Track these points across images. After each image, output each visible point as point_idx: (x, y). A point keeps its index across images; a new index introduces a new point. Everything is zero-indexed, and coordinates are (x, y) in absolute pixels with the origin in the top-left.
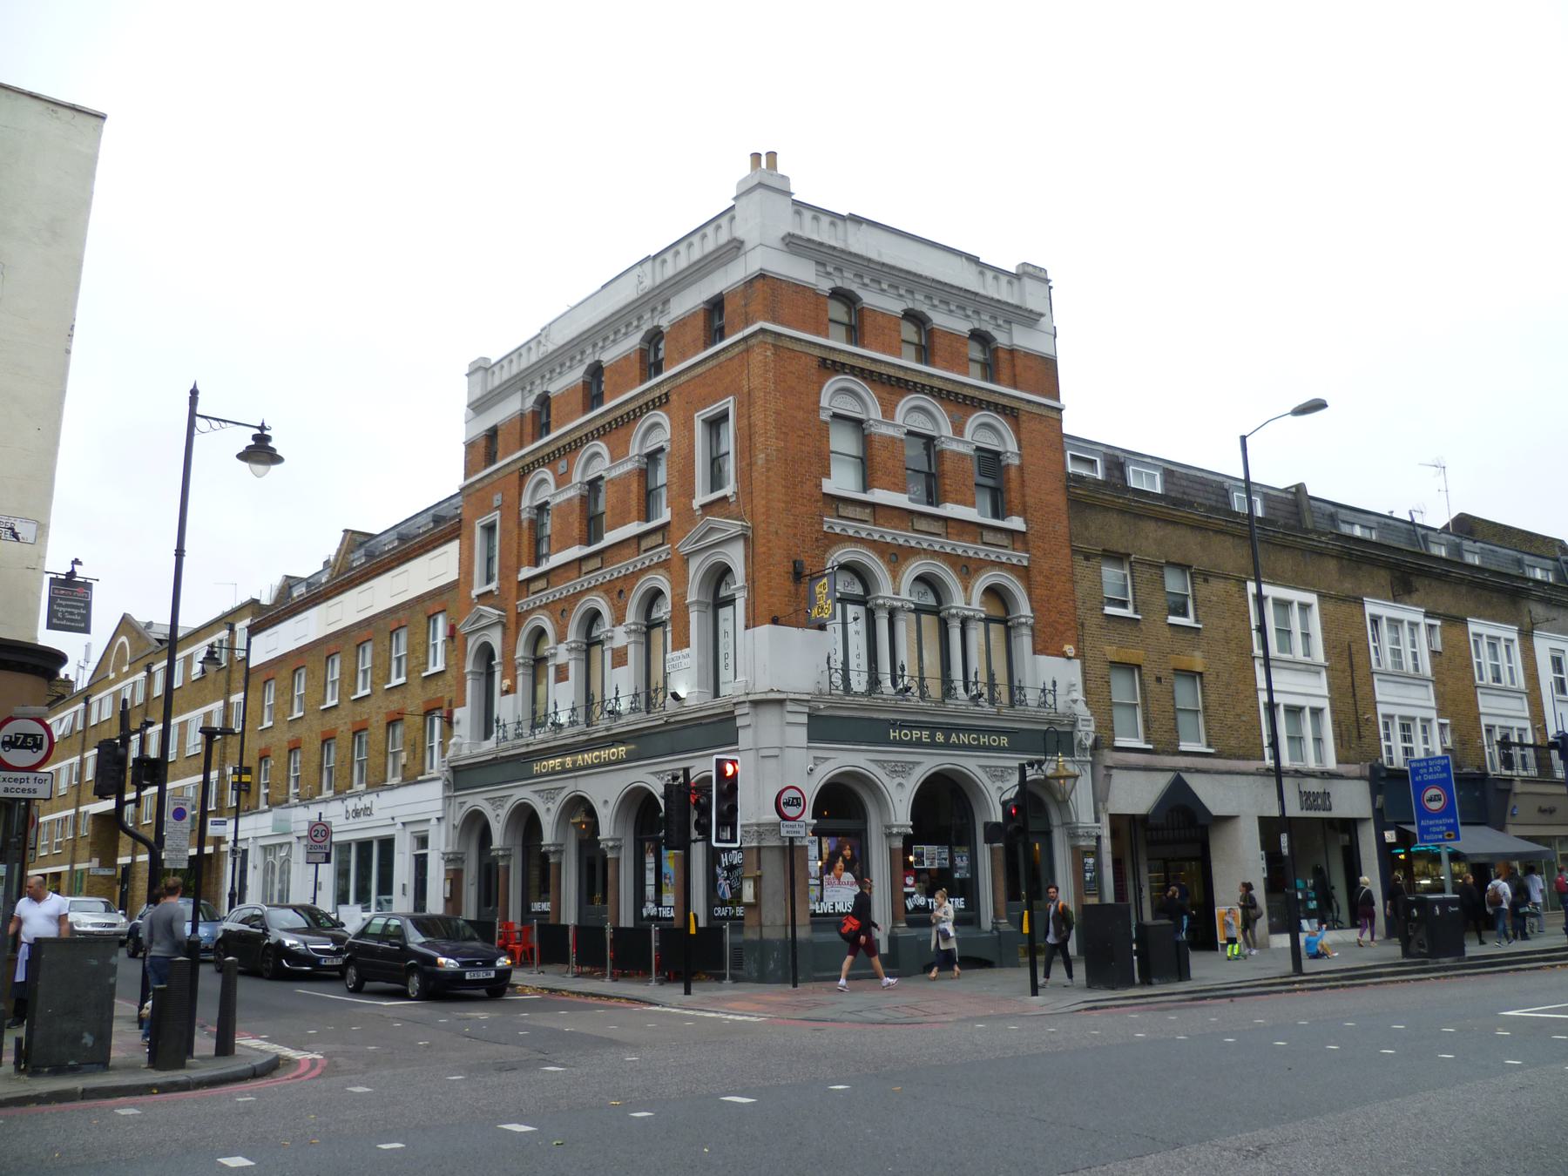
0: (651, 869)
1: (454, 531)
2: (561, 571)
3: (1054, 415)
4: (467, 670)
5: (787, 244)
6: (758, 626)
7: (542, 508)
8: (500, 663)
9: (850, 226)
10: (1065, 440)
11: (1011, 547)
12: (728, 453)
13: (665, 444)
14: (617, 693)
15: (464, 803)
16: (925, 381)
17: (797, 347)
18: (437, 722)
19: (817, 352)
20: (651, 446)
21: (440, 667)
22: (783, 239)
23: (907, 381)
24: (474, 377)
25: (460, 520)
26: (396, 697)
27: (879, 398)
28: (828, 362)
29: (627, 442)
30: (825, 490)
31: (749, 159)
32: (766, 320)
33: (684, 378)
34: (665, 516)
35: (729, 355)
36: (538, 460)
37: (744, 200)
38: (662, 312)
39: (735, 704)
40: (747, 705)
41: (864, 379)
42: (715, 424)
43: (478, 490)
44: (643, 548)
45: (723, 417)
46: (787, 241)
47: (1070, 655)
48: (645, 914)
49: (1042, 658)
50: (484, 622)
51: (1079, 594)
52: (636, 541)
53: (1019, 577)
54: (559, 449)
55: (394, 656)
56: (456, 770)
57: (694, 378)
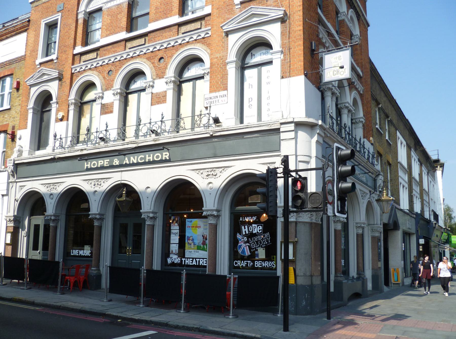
0: (175, 234)
2: (110, 47)
4: (29, 107)
14: (107, 127)
39: (282, 124)
40: (293, 125)
44: (82, 60)
48: (169, 261)
50: (45, 78)
52: (80, 55)
56: (16, 166)
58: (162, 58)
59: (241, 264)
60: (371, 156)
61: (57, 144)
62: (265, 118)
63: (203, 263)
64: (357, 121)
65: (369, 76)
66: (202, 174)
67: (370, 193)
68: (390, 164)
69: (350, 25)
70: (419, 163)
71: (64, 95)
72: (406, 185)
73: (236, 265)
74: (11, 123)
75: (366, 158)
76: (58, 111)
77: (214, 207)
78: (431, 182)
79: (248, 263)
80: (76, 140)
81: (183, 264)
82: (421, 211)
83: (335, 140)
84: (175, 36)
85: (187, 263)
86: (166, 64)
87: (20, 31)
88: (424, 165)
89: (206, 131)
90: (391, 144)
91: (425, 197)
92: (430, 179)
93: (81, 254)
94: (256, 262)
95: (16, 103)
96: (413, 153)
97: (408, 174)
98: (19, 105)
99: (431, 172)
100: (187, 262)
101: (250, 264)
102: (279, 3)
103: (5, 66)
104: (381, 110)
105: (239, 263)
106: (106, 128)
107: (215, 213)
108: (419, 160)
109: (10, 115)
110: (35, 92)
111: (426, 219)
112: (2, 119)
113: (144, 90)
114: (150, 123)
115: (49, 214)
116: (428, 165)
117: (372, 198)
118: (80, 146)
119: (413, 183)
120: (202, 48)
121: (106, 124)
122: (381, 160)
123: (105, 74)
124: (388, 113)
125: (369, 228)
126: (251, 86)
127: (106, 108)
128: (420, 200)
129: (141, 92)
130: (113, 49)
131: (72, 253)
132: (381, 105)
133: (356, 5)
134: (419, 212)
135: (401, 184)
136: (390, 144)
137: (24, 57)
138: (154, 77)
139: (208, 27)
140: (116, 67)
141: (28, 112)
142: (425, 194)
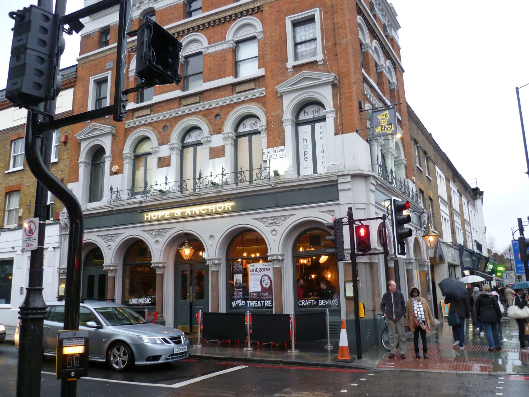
1: (71, 83)
2: (164, 104)
4: (80, 161)
6: (346, 133)
12: (106, 97)
14: (166, 180)
25: (76, 77)
26: (15, 177)
39: (338, 176)
40: (350, 176)
42: (100, 83)
43: (92, 60)
45: (105, 80)
55: (12, 155)
58: (217, 115)
59: (305, 303)
60: (415, 195)
61: (114, 197)
62: (321, 170)
63: (268, 304)
64: (399, 162)
65: (407, 119)
66: (265, 222)
67: (416, 230)
68: (431, 199)
69: (388, 75)
70: (459, 194)
71: (118, 150)
72: (448, 218)
73: (300, 304)
74: (60, 176)
75: (411, 198)
76: (112, 165)
77: (279, 252)
78: (471, 211)
79: (312, 302)
80: (133, 193)
81: (248, 306)
82: (464, 242)
83: (385, 186)
84: (230, 96)
85: (252, 305)
86: (222, 120)
87: (66, 86)
88: (464, 195)
89: (268, 183)
90: (431, 179)
91: (467, 228)
92: (470, 209)
93: (140, 303)
94: (319, 300)
95: (64, 157)
96: (452, 185)
97: (448, 206)
98: (68, 158)
99: (472, 201)
100: (252, 304)
101: (314, 303)
102: (328, 68)
104: (420, 149)
105: (330, 302)
106: (166, 181)
107: (280, 258)
108: (458, 191)
109: (58, 169)
110: (85, 147)
111: (469, 250)
113: (200, 144)
114: (211, 176)
115: (106, 265)
116: (468, 194)
117: (418, 235)
118: (139, 198)
119: (454, 214)
120: (257, 106)
121: (166, 178)
122: (423, 197)
123: (161, 129)
124: (426, 151)
125: (417, 263)
126: (305, 141)
127: (162, 161)
128: (462, 231)
129: (197, 146)
130: (168, 106)
131: (131, 302)
132: (419, 144)
133: (392, 56)
134: (462, 244)
135: (442, 217)
136: (430, 180)
137: (72, 112)
138: (211, 133)
139: (262, 88)
141: (79, 165)
142: (467, 224)
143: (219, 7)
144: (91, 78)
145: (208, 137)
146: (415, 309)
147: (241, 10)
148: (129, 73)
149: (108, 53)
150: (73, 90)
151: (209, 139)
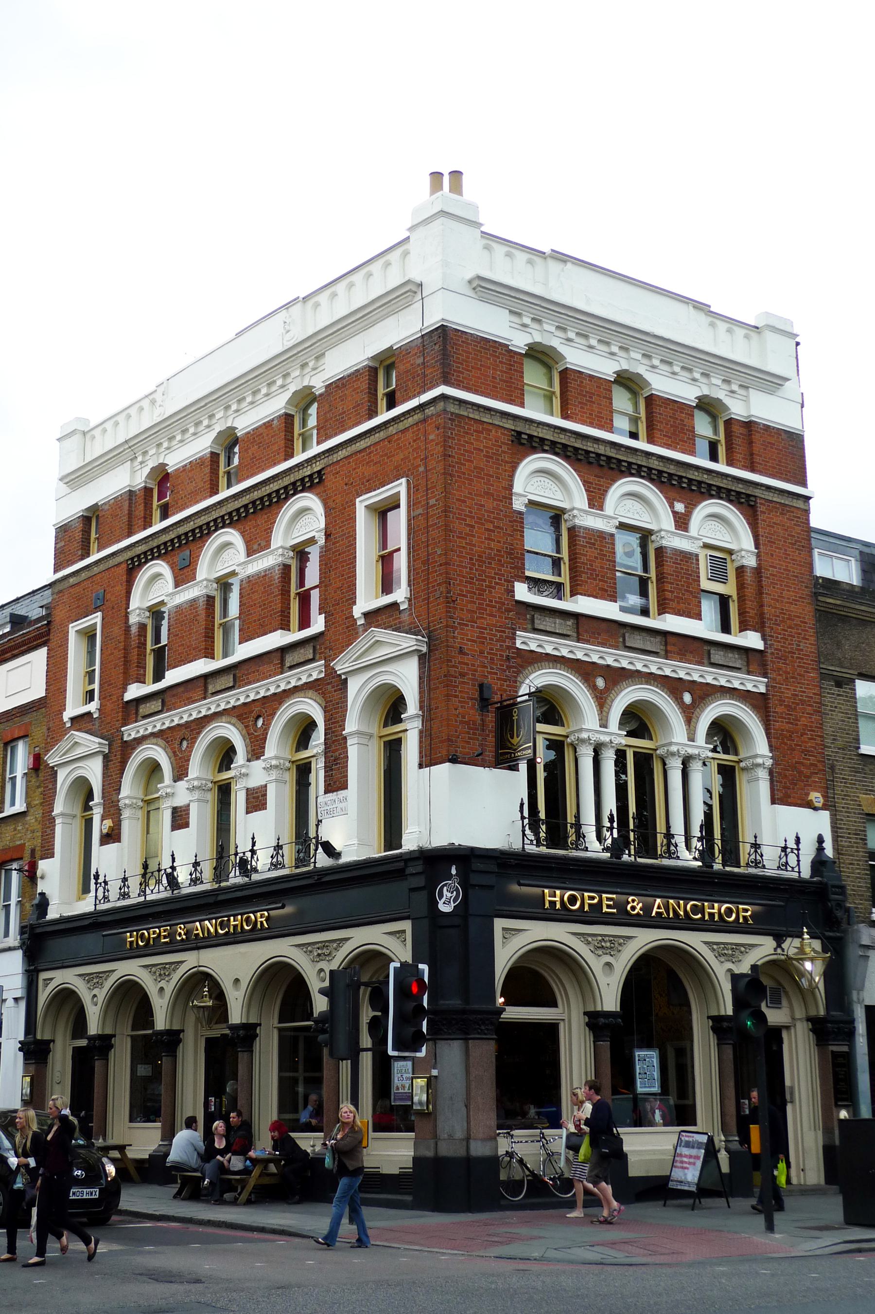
1: (41, 636)
3: (800, 504)
5: (474, 289)
7: (156, 613)
8: (99, 804)
9: (554, 267)
10: (813, 535)
11: (744, 669)
13: (317, 535)
14: (254, 844)
15: (51, 979)
16: (723, 484)
17: (486, 419)
18: (15, 875)
19: (509, 425)
20: (298, 536)
21: (20, 806)
22: (470, 282)
23: (620, 461)
24: (67, 443)
25: (49, 623)
27: (586, 483)
28: (524, 436)
29: (269, 531)
30: (517, 598)
31: (427, 180)
32: (447, 382)
33: (342, 454)
34: (318, 624)
35: (401, 426)
36: (152, 550)
37: (422, 231)
38: (314, 369)
41: (566, 458)
46: (474, 285)
47: (817, 805)
49: (783, 810)
50: (79, 752)
51: (828, 729)
52: (279, 654)
53: (755, 707)
54: (179, 537)
57: (356, 453)
103: (13, 717)
106: (173, 863)
112: (13, 833)
127: (179, 816)
130: (187, 695)
140: (192, 731)
141: (346, 743)
143: (263, 470)
144: (71, 625)
145: (242, 766)
146: (723, 1143)
147: (292, 480)
148: (130, 616)
149: (96, 570)
150: (46, 652)
151: (243, 770)
